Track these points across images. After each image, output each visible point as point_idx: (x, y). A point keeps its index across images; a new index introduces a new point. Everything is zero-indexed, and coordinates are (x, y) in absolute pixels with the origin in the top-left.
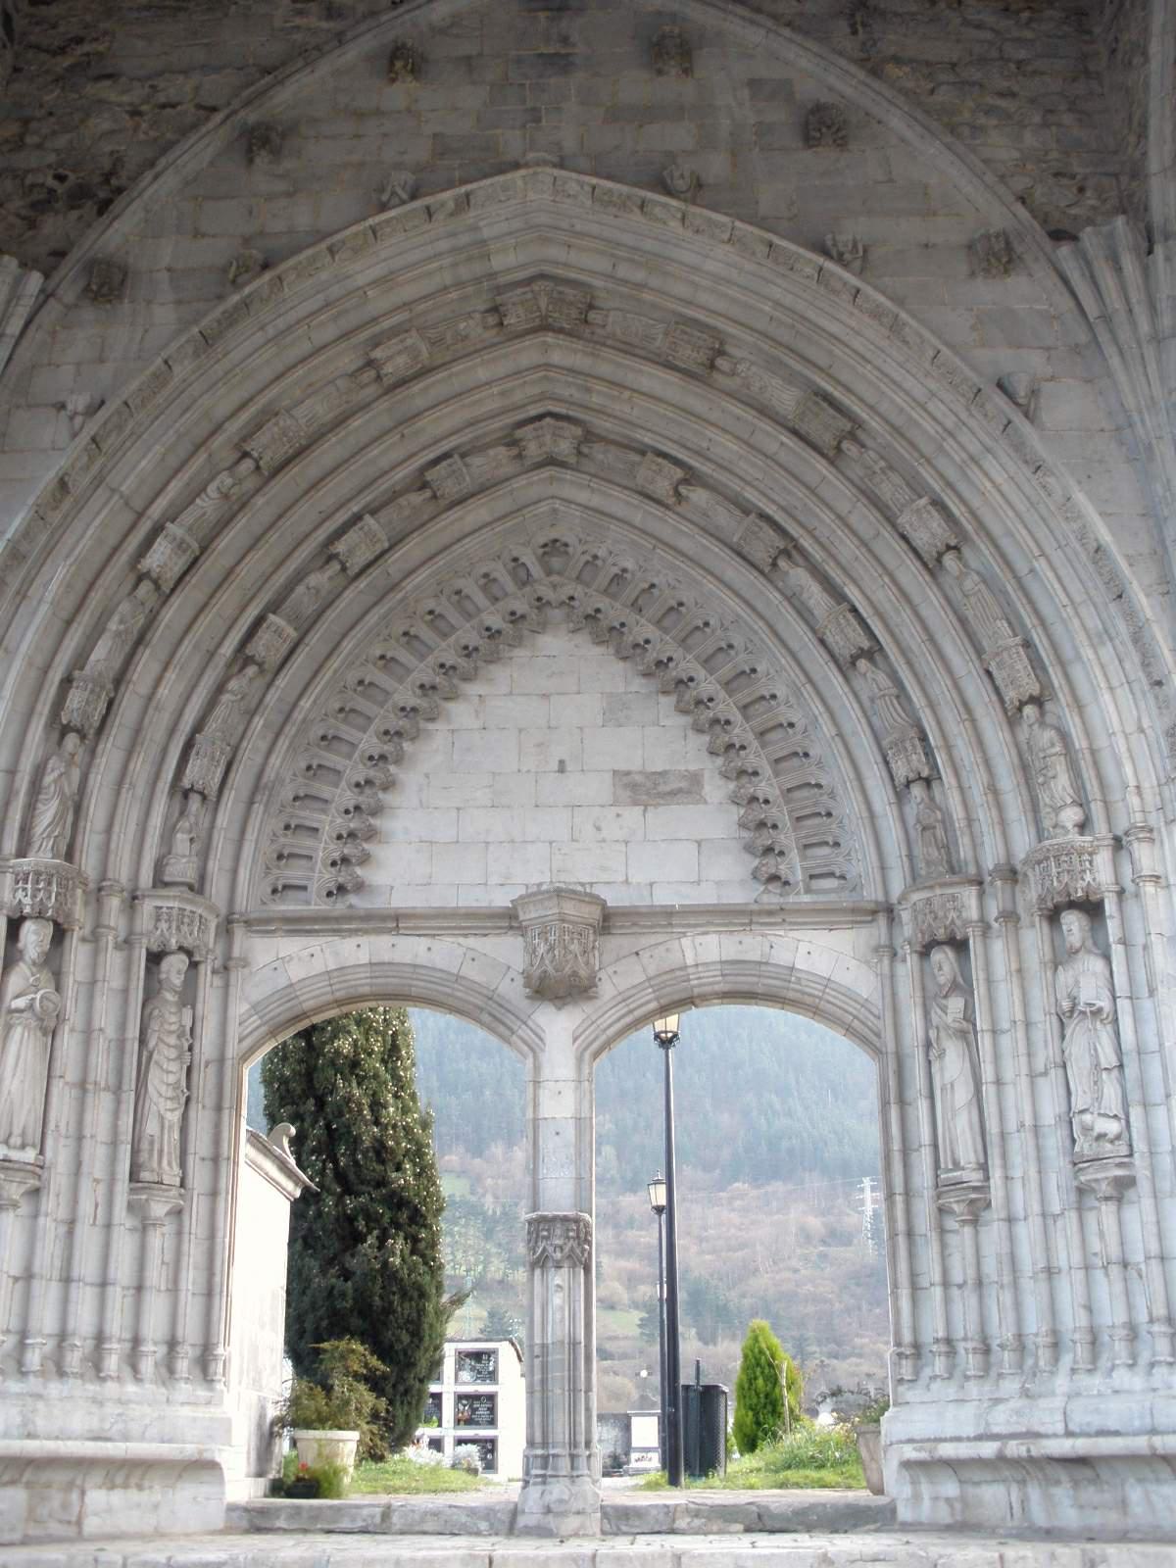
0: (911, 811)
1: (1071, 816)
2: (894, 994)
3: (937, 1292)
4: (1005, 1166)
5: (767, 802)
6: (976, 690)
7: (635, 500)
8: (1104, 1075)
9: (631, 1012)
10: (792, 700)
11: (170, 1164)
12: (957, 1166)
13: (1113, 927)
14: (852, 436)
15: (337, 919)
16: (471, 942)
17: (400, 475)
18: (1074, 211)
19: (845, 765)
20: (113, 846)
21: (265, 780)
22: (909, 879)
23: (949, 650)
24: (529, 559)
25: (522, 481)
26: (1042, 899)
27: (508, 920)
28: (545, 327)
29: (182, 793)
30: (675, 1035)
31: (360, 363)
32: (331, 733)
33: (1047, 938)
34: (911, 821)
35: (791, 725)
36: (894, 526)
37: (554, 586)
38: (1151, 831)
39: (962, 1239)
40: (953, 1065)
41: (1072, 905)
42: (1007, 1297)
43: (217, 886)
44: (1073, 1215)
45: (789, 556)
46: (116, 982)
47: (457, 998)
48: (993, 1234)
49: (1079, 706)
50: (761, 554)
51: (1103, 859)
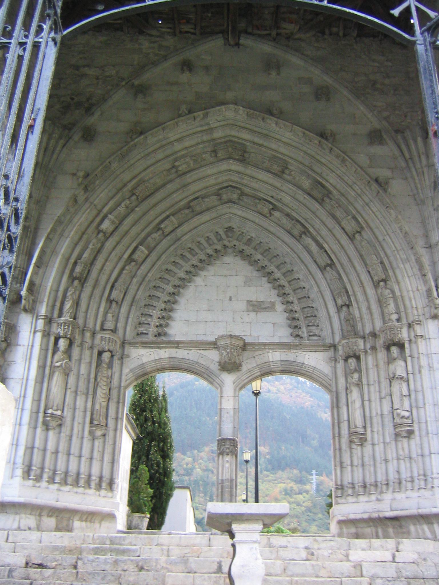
0: (343, 315)
1: (394, 317)
2: (336, 373)
3: (349, 468)
4: (371, 427)
5: (296, 312)
6: (365, 277)
7: (257, 215)
8: (404, 398)
9: (252, 375)
10: (305, 280)
11: (103, 419)
12: (356, 427)
13: (407, 351)
14: (328, 196)
15: (159, 343)
16: (202, 352)
17: (182, 203)
18: (403, 124)
19: (321, 300)
20: (88, 316)
21: (136, 298)
22: (341, 337)
23: (356, 264)
24: (221, 232)
25: (220, 208)
26: (384, 342)
27: (214, 345)
28: (229, 158)
29: (110, 301)
30: (259, 392)
31: (170, 166)
32: (157, 285)
33: (386, 355)
34: (342, 318)
35: (304, 288)
36: (340, 225)
37: (229, 241)
38: (420, 321)
39: (357, 450)
40: (355, 394)
41: (394, 344)
42: (372, 469)
43: (120, 332)
44: (393, 443)
45: (305, 234)
46: (88, 360)
47: (197, 369)
48: (368, 448)
49: (398, 283)
50: (296, 232)
51: (405, 331)
